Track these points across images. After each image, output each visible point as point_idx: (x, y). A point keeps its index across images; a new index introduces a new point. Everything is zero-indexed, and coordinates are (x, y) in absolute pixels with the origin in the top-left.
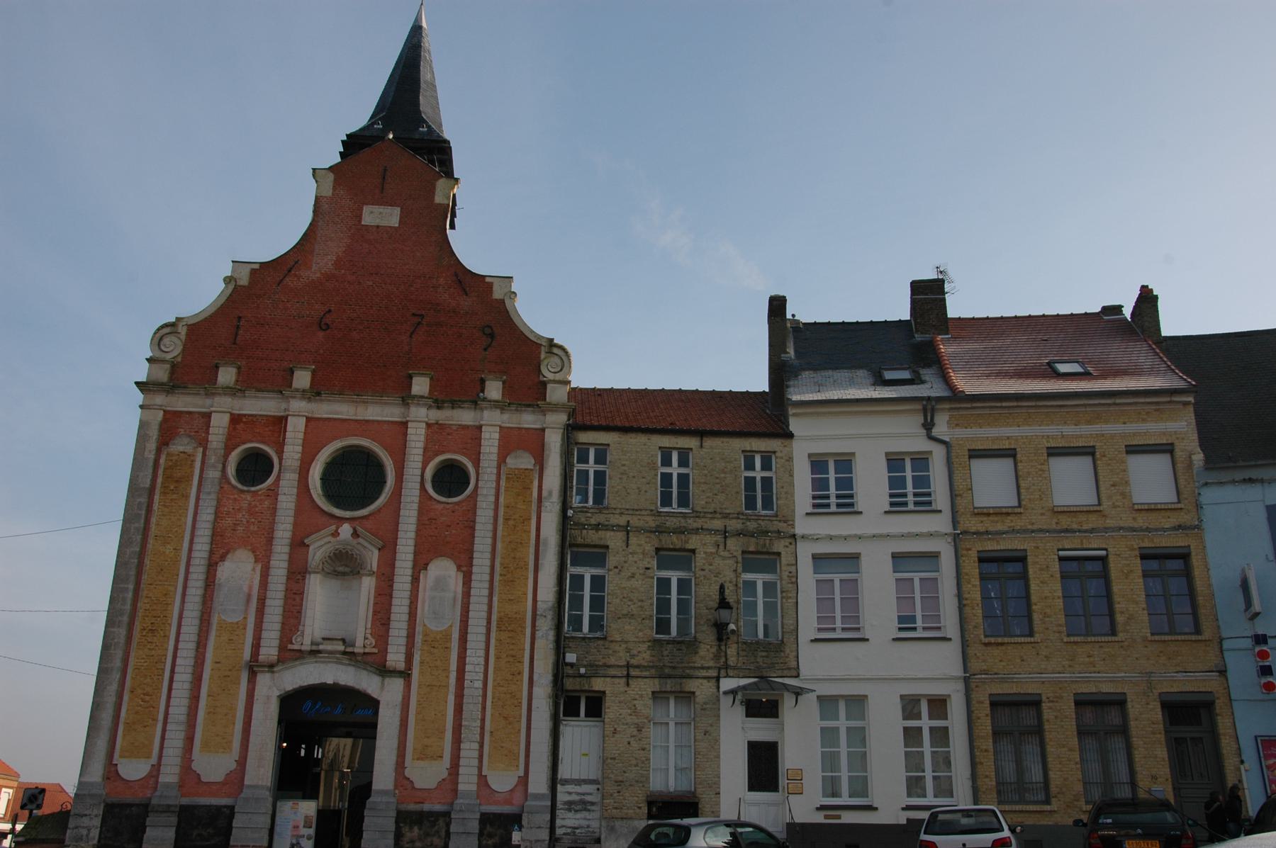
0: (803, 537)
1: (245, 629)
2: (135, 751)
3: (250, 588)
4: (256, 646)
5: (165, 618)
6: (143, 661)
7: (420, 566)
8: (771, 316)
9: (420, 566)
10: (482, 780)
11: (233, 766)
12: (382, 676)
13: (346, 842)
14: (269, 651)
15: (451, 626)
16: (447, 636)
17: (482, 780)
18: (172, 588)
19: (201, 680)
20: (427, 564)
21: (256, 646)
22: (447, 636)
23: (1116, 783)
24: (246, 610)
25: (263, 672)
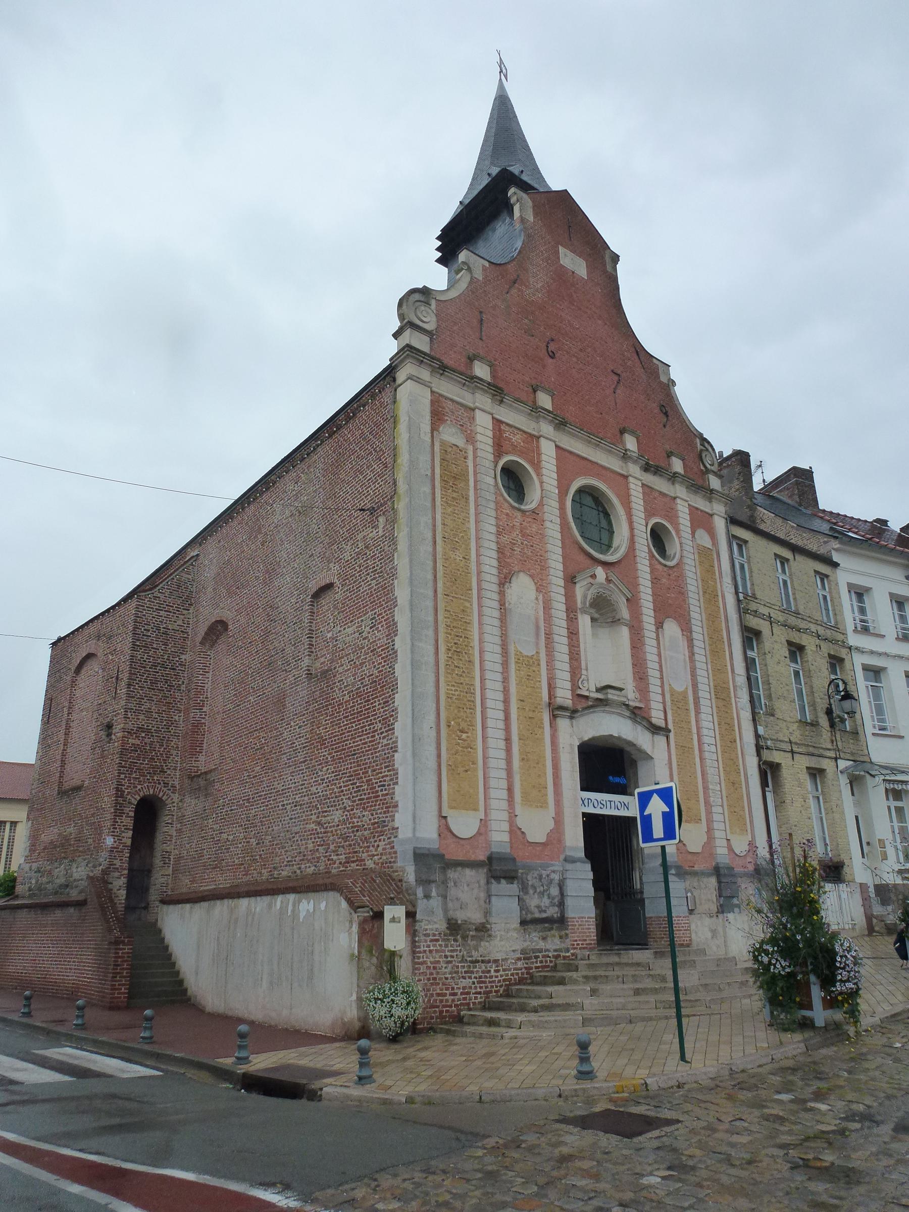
0: (856, 649)
1: (539, 665)
2: (466, 802)
3: (537, 619)
4: (551, 688)
5: (466, 639)
6: (453, 688)
7: (659, 625)
8: (813, 499)
9: (659, 625)
10: (730, 849)
11: (551, 825)
12: (653, 733)
13: (1, 1088)
14: (564, 696)
15: (687, 688)
16: (685, 693)
17: (730, 849)
18: (468, 605)
19: (705, 803)
20: (663, 624)
21: (551, 688)
22: (685, 693)
23: (14, 918)
24: (537, 644)
25: (564, 717)
